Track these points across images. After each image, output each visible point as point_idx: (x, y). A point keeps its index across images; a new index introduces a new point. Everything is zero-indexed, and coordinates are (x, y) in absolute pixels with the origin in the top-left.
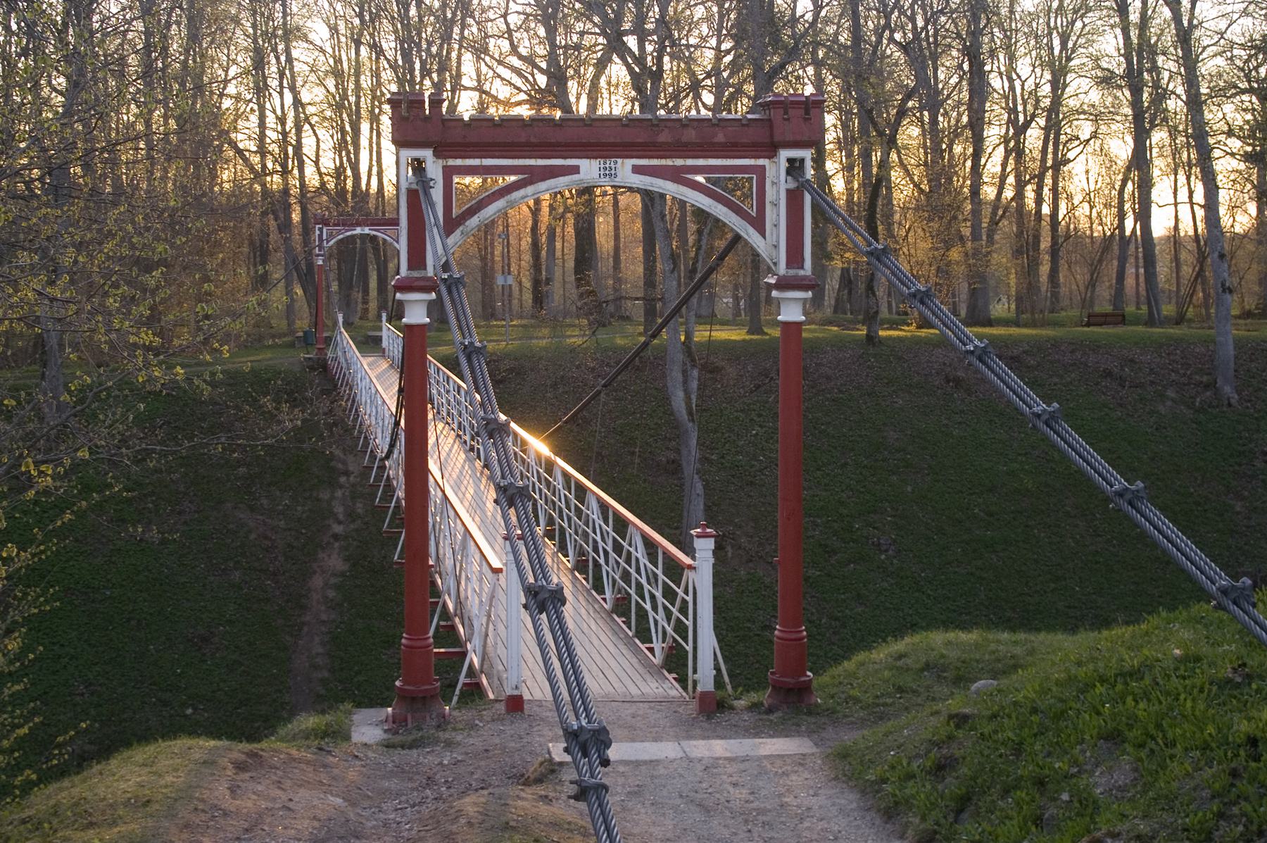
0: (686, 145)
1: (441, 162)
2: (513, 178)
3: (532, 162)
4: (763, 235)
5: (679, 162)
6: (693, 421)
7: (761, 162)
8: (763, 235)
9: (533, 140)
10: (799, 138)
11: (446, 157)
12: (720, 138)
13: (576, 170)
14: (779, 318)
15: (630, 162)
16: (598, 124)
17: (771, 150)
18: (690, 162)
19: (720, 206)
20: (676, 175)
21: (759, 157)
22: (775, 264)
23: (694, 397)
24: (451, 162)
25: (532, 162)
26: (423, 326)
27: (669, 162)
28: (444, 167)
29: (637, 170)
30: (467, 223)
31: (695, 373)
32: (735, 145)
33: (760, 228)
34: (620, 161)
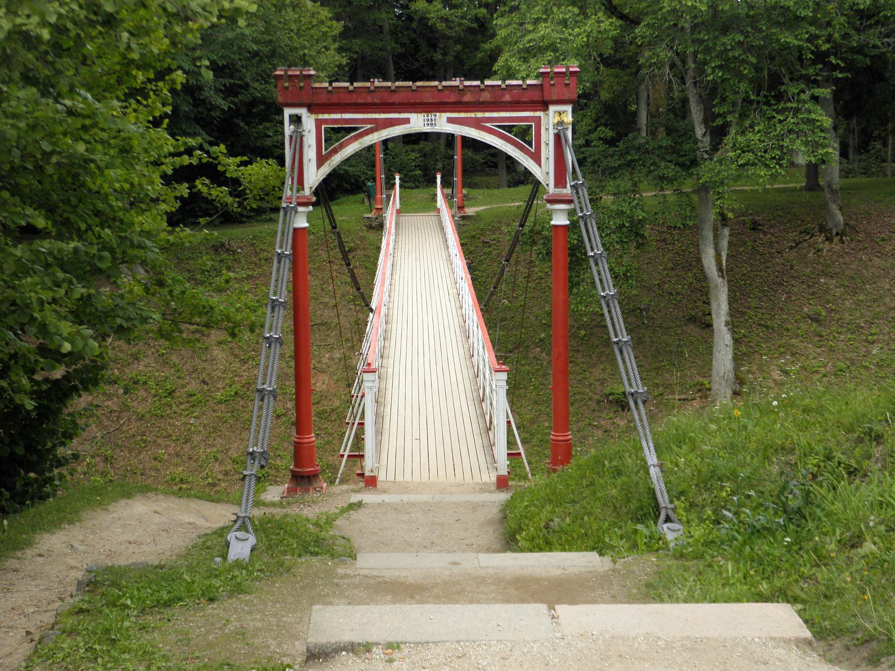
0: (483, 103)
1: (314, 117)
2: (369, 126)
3: (377, 116)
4: (540, 165)
5: (480, 115)
6: (723, 277)
7: (538, 114)
8: (540, 165)
9: (376, 101)
10: (561, 98)
11: (317, 113)
12: (507, 98)
13: (407, 121)
14: (553, 223)
15: (446, 115)
16: (421, 89)
17: (544, 105)
18: (488, 115)
19: (509, 145)
20: (477, 124)
21: (536, 111)
22: (547, 185)
23: (724, 258)
24: (321, 116)
25: (377, 116)
26: (305, 229)
27: (472, 115)
28: (316, 120)
29: (450, 121)
30: (333, 158)
31: (726, 232)
32: (518, 102)
33: (538, 162)
34: (438, 114)
